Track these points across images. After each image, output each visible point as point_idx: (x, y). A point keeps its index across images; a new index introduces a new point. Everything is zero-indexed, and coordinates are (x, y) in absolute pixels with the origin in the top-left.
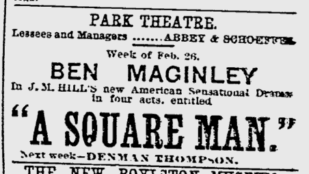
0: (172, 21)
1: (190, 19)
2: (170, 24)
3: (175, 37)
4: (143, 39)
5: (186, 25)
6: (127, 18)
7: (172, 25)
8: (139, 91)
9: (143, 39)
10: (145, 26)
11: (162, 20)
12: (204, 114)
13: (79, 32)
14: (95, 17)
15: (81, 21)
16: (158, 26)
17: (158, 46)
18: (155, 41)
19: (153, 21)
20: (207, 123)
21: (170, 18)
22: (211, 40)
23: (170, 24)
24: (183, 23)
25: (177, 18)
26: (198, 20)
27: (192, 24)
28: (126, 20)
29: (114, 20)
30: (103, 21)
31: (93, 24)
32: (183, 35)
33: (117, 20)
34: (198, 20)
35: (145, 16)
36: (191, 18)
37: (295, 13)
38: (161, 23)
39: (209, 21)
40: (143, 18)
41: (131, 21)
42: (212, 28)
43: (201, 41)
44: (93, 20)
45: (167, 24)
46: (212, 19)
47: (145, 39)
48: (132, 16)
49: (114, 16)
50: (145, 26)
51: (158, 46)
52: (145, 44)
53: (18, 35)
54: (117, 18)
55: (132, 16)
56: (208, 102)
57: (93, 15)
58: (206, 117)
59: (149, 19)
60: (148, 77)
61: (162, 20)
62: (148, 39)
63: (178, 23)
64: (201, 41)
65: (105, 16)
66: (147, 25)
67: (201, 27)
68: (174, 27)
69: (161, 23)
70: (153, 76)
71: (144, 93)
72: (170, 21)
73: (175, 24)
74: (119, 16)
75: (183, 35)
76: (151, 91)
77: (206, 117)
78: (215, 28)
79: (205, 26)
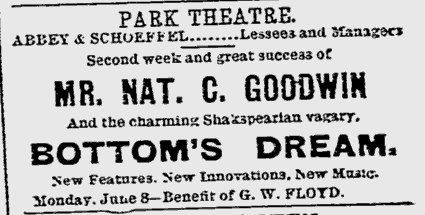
0: (233, 16)
1: (257, 11)
2: (231, 20)
3: (28, 40)
4: (199, 39)
5: (252, 20)
6: (169, 14)
7: (233, 21)
8: (78, 124)
9: (211, 39)
10: (195, 24)
11: (218, 15)
12: (256, 140)
13: (334, 29)
14: (126, 16)
15: (107, 19)
16: (214, 24)
17: (225, 46)
18: (208, 40)
19: (207, 17)
20: (182, 154)
21: (230, 10)
22: (76, 41)
23: (231, 20)
24: (249, 17)
25: (240, 11)
26: (270, 12)
27: (261, 17)
28: (169, 18)
29: (153, 19)
30: (138, 21)
31: (123, 26)
32: (39, 36)
33: (156, 19)
34: (270, 12)
35: (255, 9)
36: (199, 11)
37: (13, 6)
38: (219, 19)
39: (226, 13)
40: (192, 13)
41: (175, 17)
42: (289, 21)
43: (65, 43)
44: (123, 19)
45: (226, 20)
46: (289, 9)
47: (214, 38)
48: (176, 11)
49: (152, 12)
50: (195, 24)
51: (225, 46)
52: (207, 44)
53: (248, 37)
54: (155, 15)
55: (176, 11)
56: (92, 124)
57: (122, 13)
58: (185, 141)
59: (260, 13)
60: (139, 99)
61: (218, 15)
62: (224, 39)
63: (242, 18)
64: (65, 43)
65: (140, 14)
66: (197, 22)
67: (274, 21)
68: (236, 23)
69: (219, 19)
70: (144, 97)
71: (169, 125)
72: (230, 16)
73: (238, 18)
74: (159, 13)
75: (39, 36)
76: (119, 123)
77: (185, 141)
78: (294, 21)
79: (279, 20)
